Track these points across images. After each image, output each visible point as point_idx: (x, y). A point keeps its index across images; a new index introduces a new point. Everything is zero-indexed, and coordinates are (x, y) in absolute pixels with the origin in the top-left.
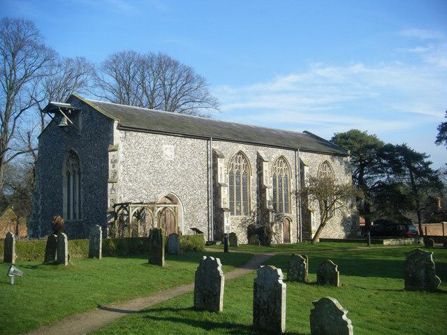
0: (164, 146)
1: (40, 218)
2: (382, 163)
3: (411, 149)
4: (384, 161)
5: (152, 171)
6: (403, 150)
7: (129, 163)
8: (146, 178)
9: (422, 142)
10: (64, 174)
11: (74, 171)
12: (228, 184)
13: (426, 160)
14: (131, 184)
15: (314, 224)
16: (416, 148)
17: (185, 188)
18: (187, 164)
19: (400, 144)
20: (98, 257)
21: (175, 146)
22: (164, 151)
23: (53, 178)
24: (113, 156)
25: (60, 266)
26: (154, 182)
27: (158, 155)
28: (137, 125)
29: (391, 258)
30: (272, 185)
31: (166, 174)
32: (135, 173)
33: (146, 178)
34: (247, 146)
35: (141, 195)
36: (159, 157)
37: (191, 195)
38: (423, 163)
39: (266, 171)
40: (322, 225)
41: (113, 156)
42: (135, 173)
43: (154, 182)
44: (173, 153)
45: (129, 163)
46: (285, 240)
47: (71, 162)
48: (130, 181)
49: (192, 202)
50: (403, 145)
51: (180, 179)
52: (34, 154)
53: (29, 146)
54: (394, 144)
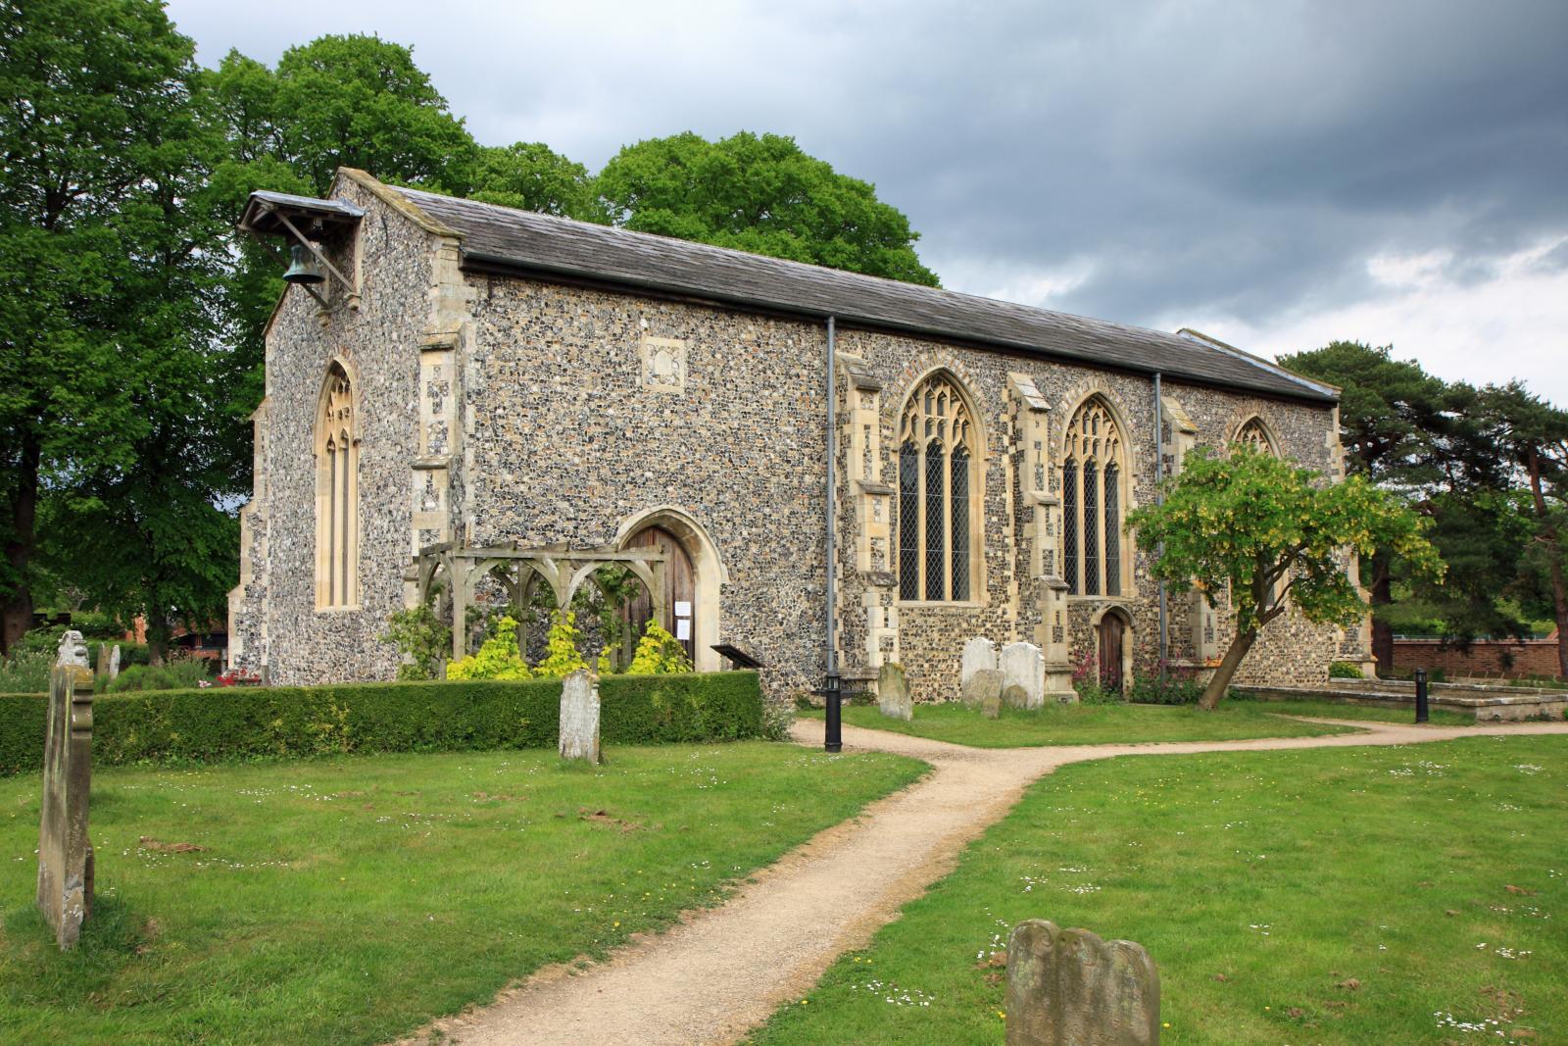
0: (649, 340)
1: (265, 601)
2: (1437, 450)
3: (1541, 401)
4: (1444, 442)
5: (595, 430)
6: (1512, 403)
7: (504, 397)
8: (573, 455)
12: (896, 486)
14: (509, 478)
15: (1209, 635)
17: (727, 496)
18: (736, 407)
19: (1501, 382)
21: (691, 343)
22: (647, 361)
24: (437, 369)
26: (605, 472)
27: (621, 373)
28: (831, 277)
29: (958, 748)
30: (1060, 495)
31: (654, 445)
32: (529, 438)
34: (971, 355)
35: (547, 519)
36: (629, 378)
37: (753, 524)
39: (1038, 445)
40: (1245, 640)
41: (437, 369)
42: (529, 438)
43: (605, 472)
44: (683, 371)
45: (504, 397)
48: (506, 465)
49: (754, 549)
50: (1512, 387)
51: (709, 466)
54: (1479, 383)
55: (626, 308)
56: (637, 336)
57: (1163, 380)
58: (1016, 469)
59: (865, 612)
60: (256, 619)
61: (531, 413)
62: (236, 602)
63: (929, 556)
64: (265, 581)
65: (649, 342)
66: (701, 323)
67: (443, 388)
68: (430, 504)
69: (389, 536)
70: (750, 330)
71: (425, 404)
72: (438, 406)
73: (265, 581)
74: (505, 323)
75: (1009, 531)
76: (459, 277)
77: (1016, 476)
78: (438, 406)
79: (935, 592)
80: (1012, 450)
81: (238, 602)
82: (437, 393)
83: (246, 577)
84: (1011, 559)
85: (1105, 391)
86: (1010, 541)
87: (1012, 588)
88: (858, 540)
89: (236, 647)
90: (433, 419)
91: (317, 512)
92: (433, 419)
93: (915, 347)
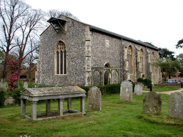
8: (100, 55)
9: (171, 48)
10: (55, 52)
11: (62, 52)
13: (172, 54)
14: (94, 58)
16: (170, 50)
20: (143, 90)
23: (49, 54)
25: (115, 96)
27: (104, 44)
31: (107, 54)
33: (100, 55)
34: (132, 43)
38: (171, 55)
41: (88, 43)
42: (96, 53)
46: (105, 83)
47: (59, 47)
52: (20, 46)
53: (18, 44)
55: (105, 36)
56: (105, 40)
57: (123, 40)
58: (136, 58)
59: (127, 75)
60: (39, 76)
61: (96, 49)
62: (36, 73)
63: (62, 66)
64: (41, 70)
65: (106, 40)
66: (110, 38)
67: (89, 46)
68: (88, 61)
69: (75, 65)
70: (114, 39)
71: (86, 48)
72: (88, 48)
73: (41, 70)
74: (94, 37)
75: (135, 65)
76: (89, 31)
77: (136, 58)
78: (88, 48)
79: (62, 73)
80: (136, 55)
81: (36, 74)
82: (88, 46)
83: (38, 70)
84: (135, 69)
85: (131, 45)
86: (135, 67)
87: (136, 72)
88: (126, 67)
89: (36, 80)
90: (87, 50)
91: (55, 61)
92: (87, 50)
93: (128, 42)
